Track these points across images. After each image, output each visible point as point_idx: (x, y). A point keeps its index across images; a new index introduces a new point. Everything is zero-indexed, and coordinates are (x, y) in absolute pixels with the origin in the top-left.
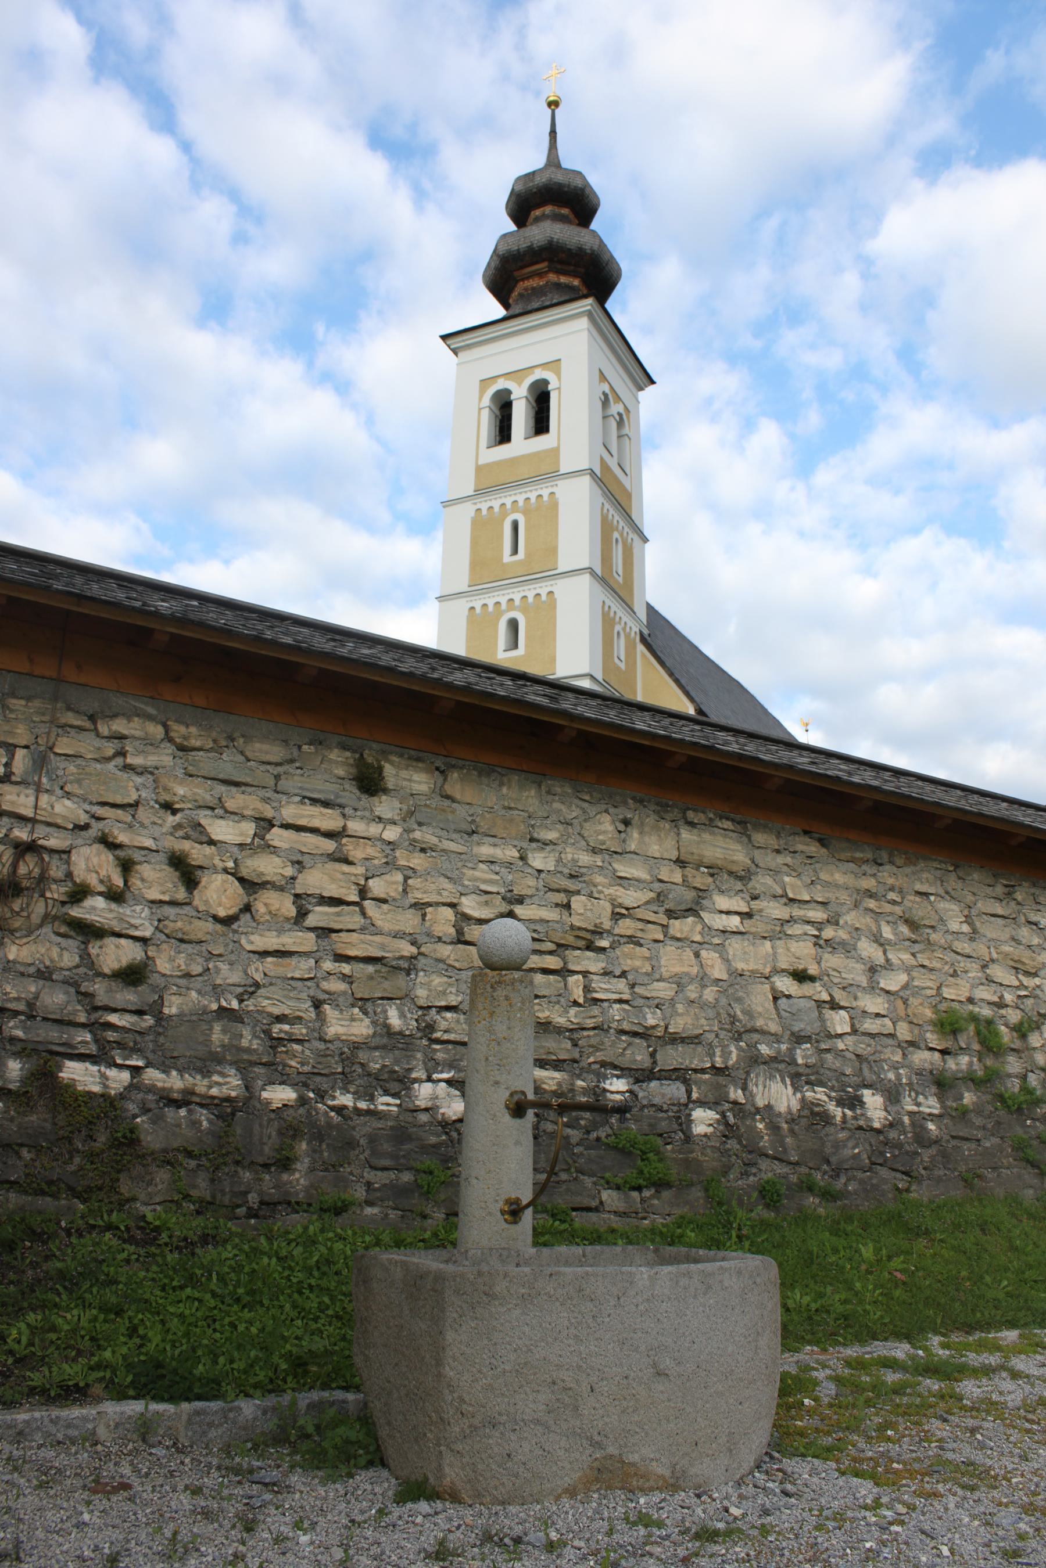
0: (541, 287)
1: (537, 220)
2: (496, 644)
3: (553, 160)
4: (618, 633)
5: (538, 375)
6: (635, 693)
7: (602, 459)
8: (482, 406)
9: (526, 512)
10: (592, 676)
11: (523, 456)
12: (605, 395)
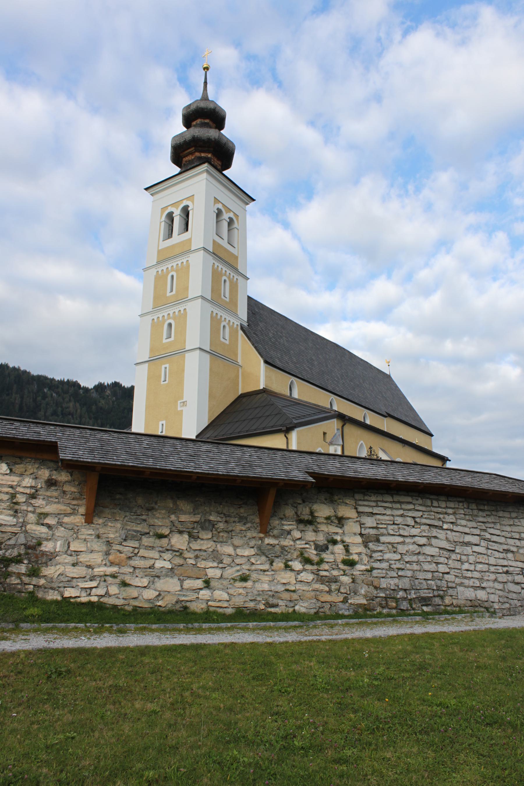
2: (163, 336)
3: (205, 97)
4: (224, 327)
5: (185, 203)
8: (162, 220)
9: (177, 271)
10: (200, 349)
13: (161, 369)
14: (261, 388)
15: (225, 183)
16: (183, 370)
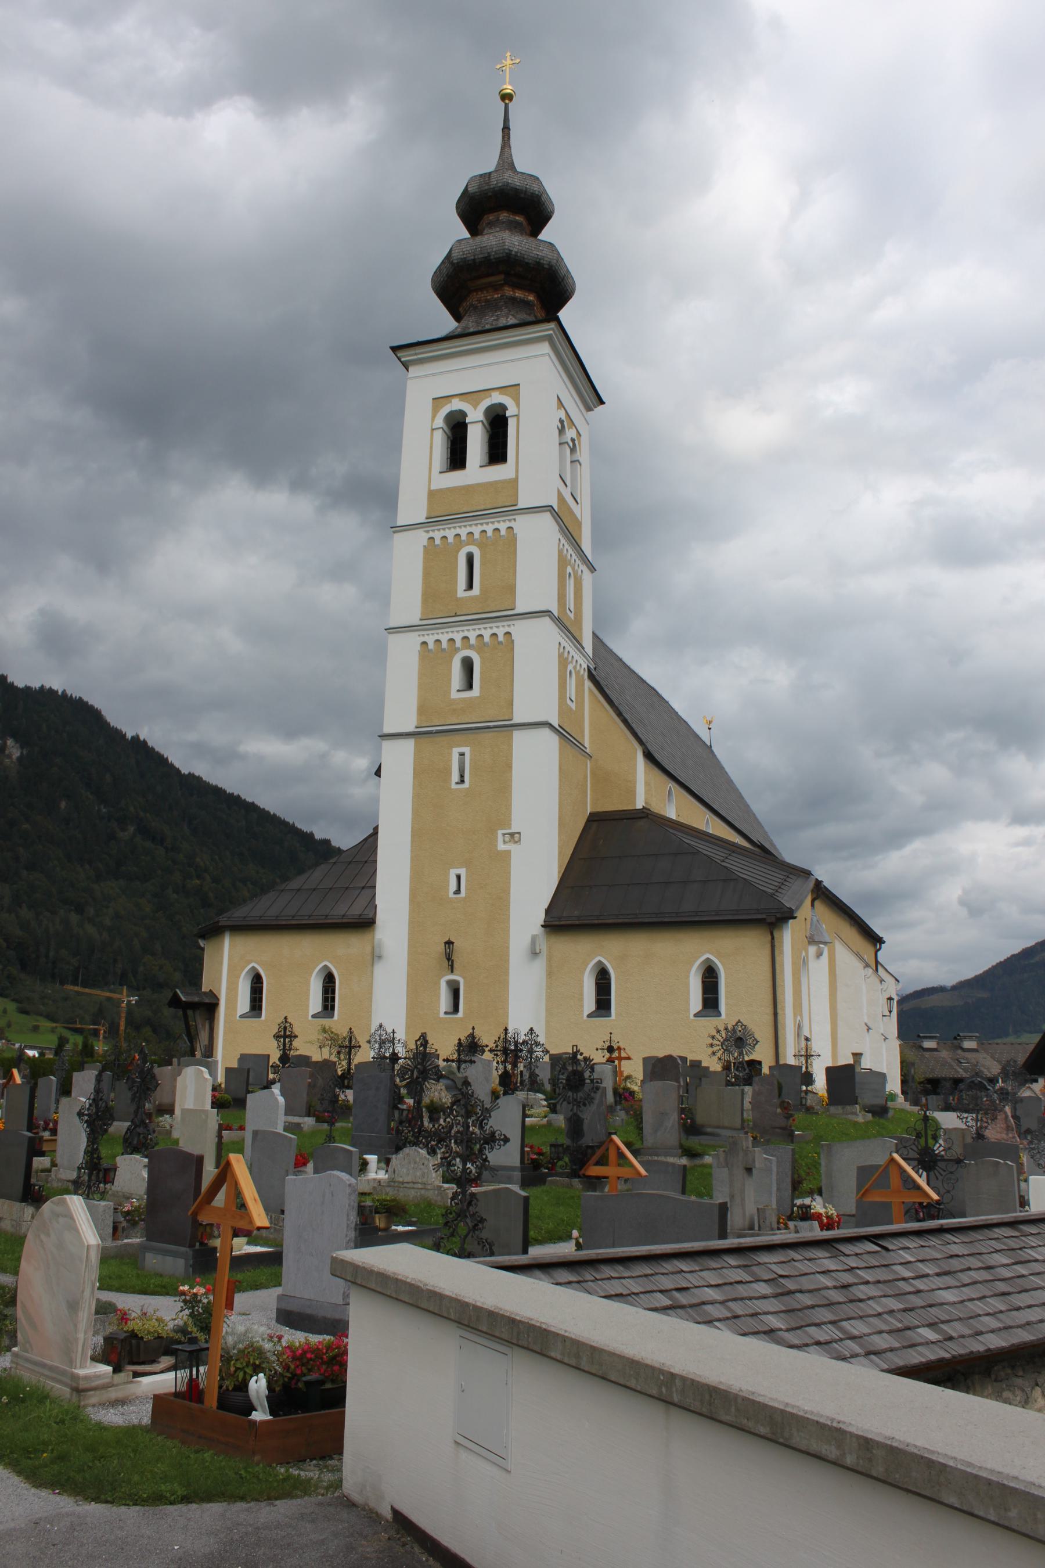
0: (496, 299)
1: (491, 225)
5: (497, 398)
6: (632, 793)
7: (559, 491)
9: (481, 545)
11: (479, 485)
12: (561, 421)
13: (450, 754)
14: (639, 806)
15: (573, 371)
16: (509, 766)
